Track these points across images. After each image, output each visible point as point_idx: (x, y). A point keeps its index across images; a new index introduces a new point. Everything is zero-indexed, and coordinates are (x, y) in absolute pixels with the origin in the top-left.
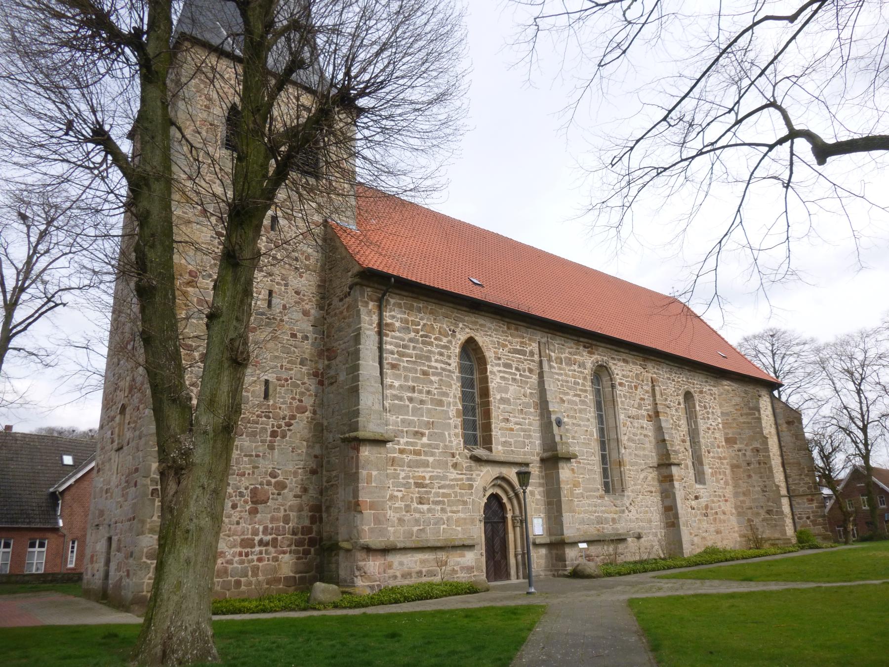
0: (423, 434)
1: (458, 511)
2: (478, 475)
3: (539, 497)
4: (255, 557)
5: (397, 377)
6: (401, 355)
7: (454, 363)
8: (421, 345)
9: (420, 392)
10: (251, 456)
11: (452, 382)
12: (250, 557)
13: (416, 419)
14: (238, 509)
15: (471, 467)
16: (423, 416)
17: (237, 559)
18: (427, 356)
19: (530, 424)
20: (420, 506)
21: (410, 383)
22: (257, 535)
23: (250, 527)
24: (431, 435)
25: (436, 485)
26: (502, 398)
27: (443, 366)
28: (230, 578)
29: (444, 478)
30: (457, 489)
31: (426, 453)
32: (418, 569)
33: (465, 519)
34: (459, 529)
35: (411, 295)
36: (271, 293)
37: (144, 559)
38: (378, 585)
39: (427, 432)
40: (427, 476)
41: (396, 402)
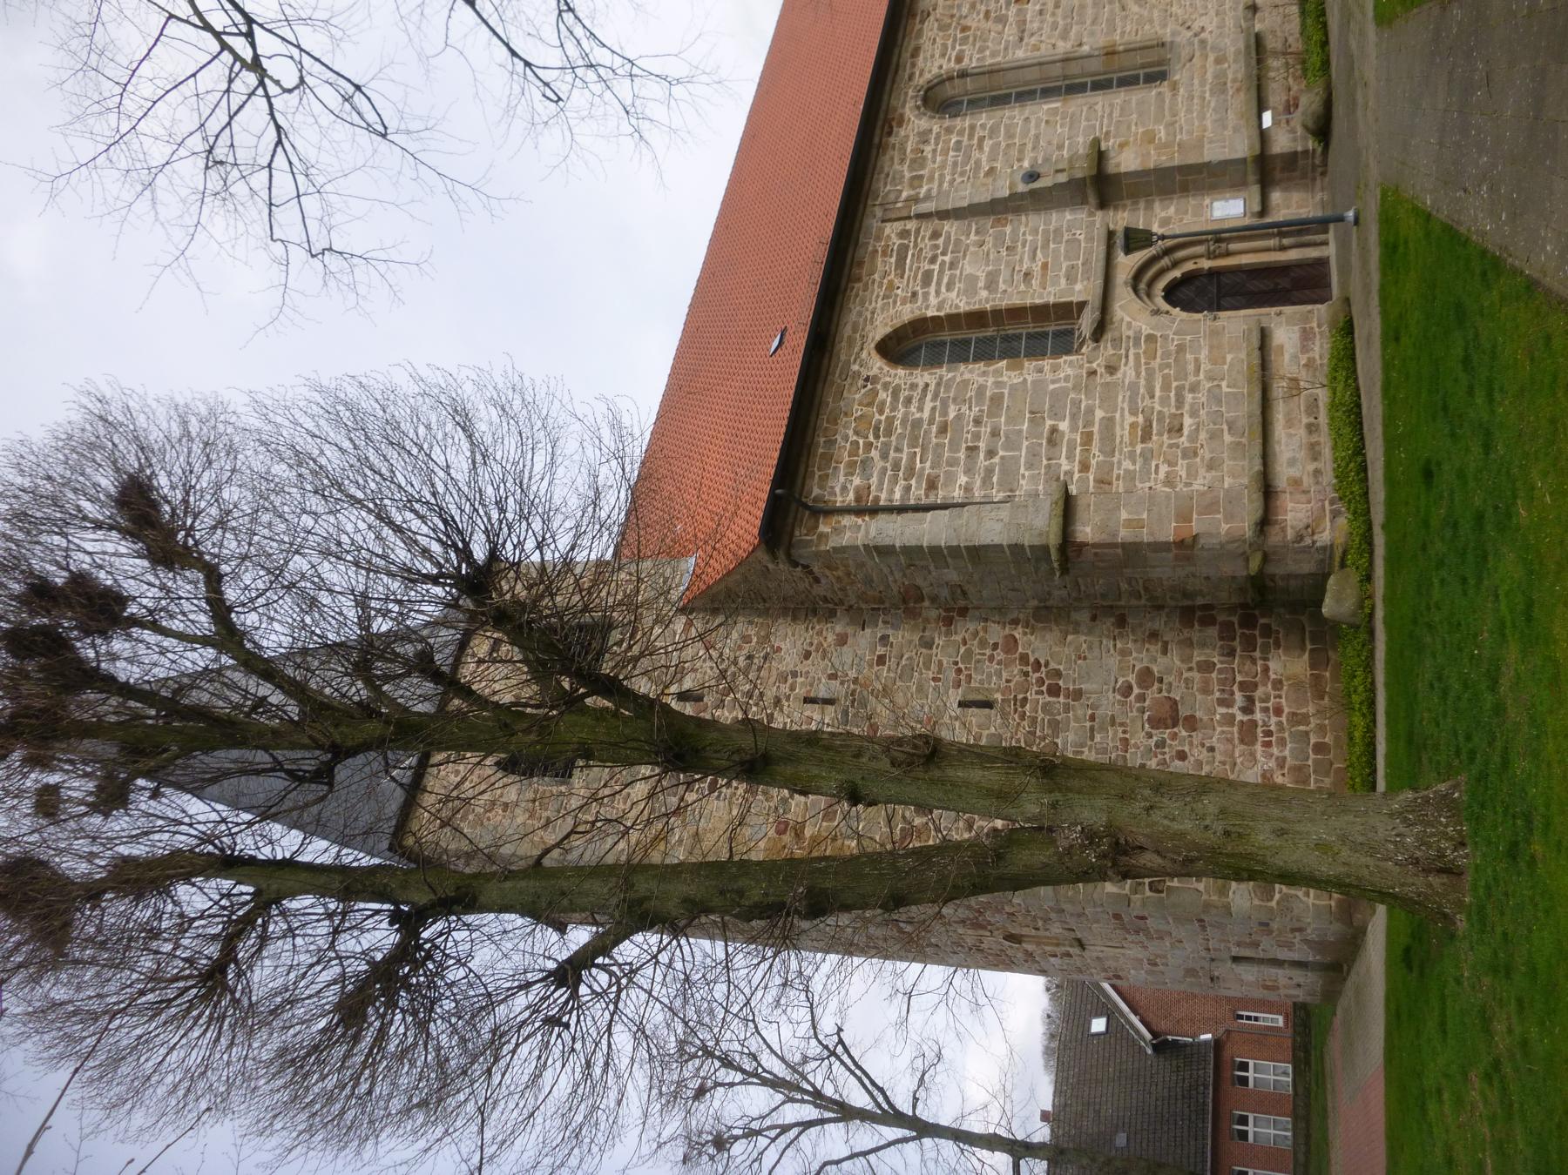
0: (1054, 430)
1: (1197, 360)
2: (1129, 325)
3: (1172, 210)
4: (1274, 719)
5: (950, 478)
7: (923, 377)
8: (893, 438)
10: (1092, 729)
12: (1272, 728)
14: (1186, 749)
16: (1021, 431)
17: (1275, 750)
20: (1186, 432)
21: (962, 455)
22: (1233, 716)
23: (1219, 729)
26: (987, 287)
27: (929, 397)
29: (1134, 387)
30: (1156, 364)
31: (1091, 423)
33: (1211, 347)
34: (1229, 357)
37: (1273, 904)
38: (1332, 503)
39: (1049, 423)
40: (1129, 419)
41: (995, 479)
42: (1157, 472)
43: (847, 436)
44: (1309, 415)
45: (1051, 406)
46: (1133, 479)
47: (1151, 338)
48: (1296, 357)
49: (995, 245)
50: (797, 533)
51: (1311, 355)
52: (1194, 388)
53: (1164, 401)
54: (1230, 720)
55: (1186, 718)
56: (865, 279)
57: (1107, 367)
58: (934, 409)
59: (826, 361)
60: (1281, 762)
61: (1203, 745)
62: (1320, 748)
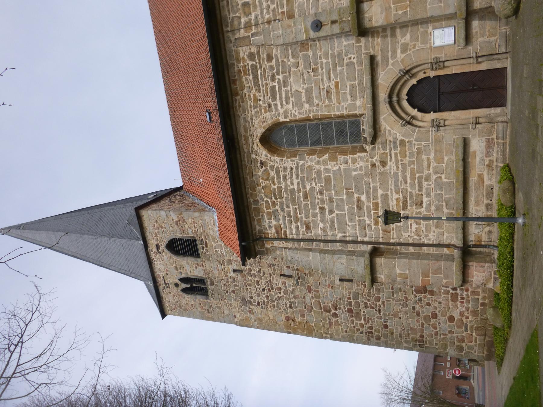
0: (359, 200)
1: (428, 159)
2: (390, 134)
3: (408, 36)
4: (465, 293)
5: (316, 225)
6: (297, 220)
7: (289, 163)
8: (284, 199)
9: (322, 201)
10: (393, 292)
11: (306, 166)
12: (464, 296)
13: (347, 207)
14: (430, 302)
15: (382, 143)
16: (343, 200)
17: (465, 304)
18: (291, 192)
19: (326, 56)
20: (424, 205)
21: (318, 211)
22: (449, 291)
23: (443, 295)
24: (359, 192)
25: (404, 186)
26: (308, 102)
27: (294, 176)
28: (479, 309)
29: (396, 175)
30: (407, 160)
31: (376, 197)
32: (484, 208)
33: (436, 151)
34: (446, 158)
35: (247, 214)
36: (281, 275)
37: (463, 354)
38: (495, 274)
39: (356, 196)
40: (396, 196)
41: (336, 226)
42: (411, 228)
43: (263, 198)
44: (487, 198)
45: (356, 186)
46: (400, 230)
47: (402, 142)
48: (483, 160)
49: (305, 67)
50: (257, 248)
51: (491, 158)
52: (427, 179)
53: (412, 185)
54: (447, 292)
55: (430, 291)
56: (240, 93)
57: (381, 162)
58: (298, 184)
59: (238, 156)
60: (467, 309)
61: (437, 301)
62: (483, 305)
